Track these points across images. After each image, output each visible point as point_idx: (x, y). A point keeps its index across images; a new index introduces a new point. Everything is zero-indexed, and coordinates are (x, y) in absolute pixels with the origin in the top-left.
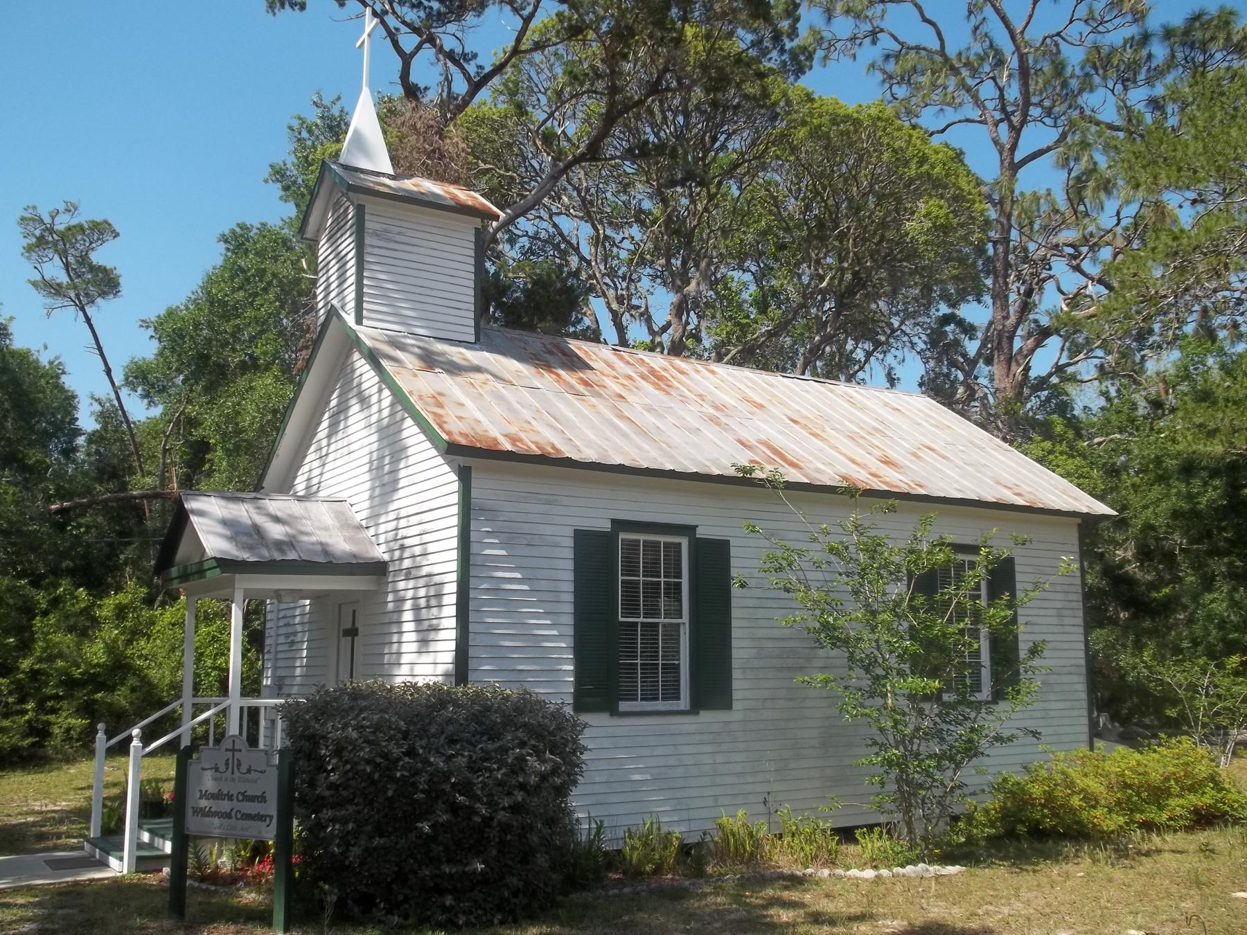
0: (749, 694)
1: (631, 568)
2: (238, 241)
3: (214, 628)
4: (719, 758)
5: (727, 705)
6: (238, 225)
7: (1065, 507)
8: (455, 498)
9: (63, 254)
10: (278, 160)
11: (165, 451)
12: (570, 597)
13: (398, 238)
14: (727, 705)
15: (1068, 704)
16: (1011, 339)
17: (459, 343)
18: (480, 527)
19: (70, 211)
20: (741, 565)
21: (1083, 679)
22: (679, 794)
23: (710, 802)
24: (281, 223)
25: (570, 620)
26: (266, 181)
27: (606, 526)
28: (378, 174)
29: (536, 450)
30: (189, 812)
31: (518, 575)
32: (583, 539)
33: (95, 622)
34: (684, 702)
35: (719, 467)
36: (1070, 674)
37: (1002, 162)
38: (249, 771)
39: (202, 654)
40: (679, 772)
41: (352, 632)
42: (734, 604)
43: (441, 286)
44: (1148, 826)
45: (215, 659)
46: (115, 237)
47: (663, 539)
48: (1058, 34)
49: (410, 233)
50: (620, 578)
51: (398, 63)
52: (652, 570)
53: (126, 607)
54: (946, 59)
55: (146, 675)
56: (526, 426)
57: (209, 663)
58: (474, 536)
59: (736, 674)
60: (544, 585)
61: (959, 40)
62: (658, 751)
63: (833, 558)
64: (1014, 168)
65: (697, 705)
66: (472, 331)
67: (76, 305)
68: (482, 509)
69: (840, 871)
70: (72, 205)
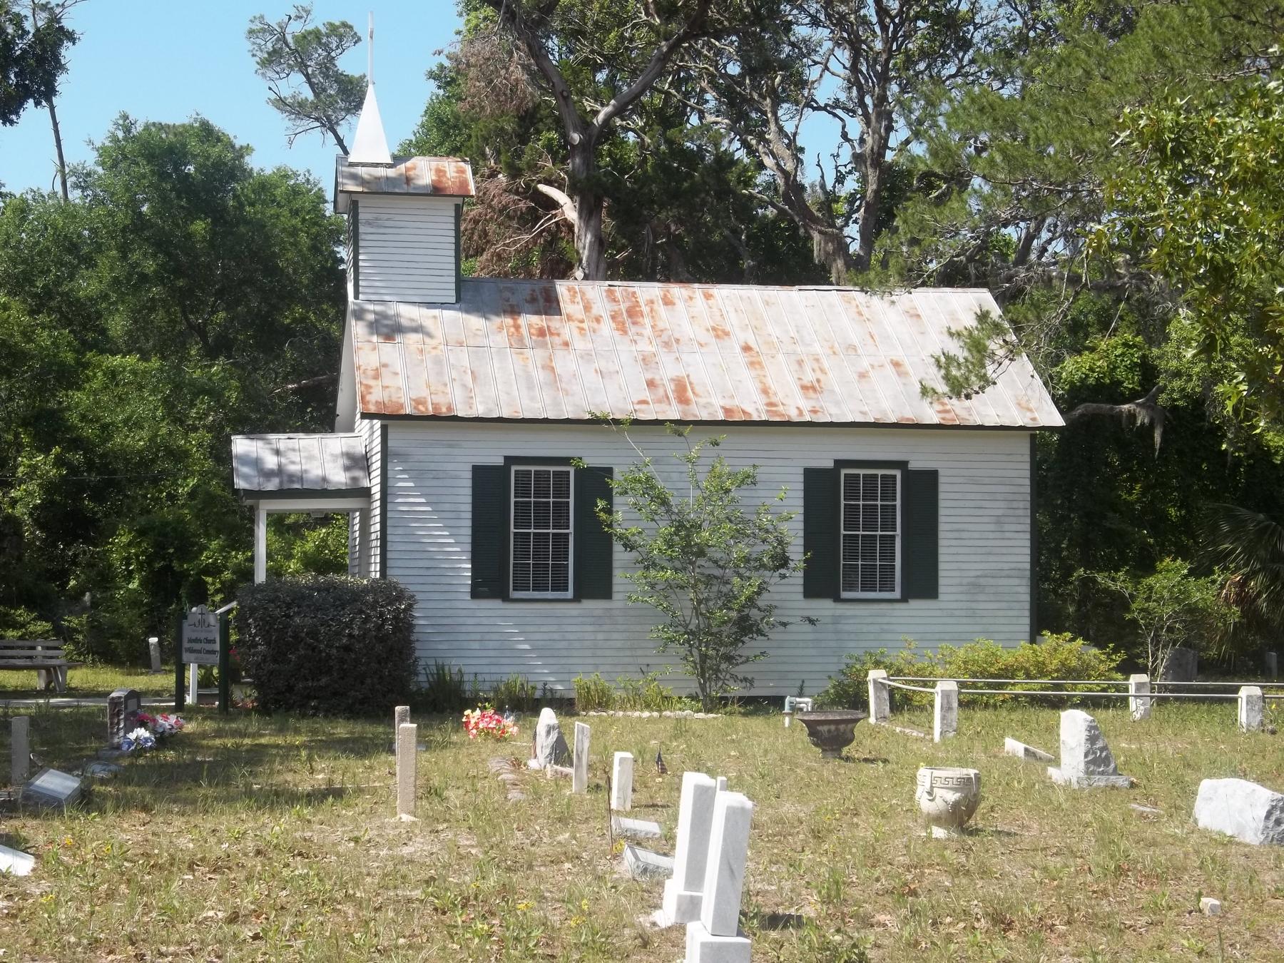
1: (523, 490)
4: (600, 636)
9: (303, 67)
12: (469, 515)
15: (1004, 605)
19: (301, 17)
21: (1026, 582)
22: (563, 661)
29: (431, 412)
31: (423, 500)
34: (570, 594)
36: (1009, 577)
46: (356, 43)
49: (398, 217)
50: (513, 500)
58: (390, 474)
65: (577, 598)
66: (453, 293)
67: (324, 125)
68: (397, 455)
70: (304, 9)
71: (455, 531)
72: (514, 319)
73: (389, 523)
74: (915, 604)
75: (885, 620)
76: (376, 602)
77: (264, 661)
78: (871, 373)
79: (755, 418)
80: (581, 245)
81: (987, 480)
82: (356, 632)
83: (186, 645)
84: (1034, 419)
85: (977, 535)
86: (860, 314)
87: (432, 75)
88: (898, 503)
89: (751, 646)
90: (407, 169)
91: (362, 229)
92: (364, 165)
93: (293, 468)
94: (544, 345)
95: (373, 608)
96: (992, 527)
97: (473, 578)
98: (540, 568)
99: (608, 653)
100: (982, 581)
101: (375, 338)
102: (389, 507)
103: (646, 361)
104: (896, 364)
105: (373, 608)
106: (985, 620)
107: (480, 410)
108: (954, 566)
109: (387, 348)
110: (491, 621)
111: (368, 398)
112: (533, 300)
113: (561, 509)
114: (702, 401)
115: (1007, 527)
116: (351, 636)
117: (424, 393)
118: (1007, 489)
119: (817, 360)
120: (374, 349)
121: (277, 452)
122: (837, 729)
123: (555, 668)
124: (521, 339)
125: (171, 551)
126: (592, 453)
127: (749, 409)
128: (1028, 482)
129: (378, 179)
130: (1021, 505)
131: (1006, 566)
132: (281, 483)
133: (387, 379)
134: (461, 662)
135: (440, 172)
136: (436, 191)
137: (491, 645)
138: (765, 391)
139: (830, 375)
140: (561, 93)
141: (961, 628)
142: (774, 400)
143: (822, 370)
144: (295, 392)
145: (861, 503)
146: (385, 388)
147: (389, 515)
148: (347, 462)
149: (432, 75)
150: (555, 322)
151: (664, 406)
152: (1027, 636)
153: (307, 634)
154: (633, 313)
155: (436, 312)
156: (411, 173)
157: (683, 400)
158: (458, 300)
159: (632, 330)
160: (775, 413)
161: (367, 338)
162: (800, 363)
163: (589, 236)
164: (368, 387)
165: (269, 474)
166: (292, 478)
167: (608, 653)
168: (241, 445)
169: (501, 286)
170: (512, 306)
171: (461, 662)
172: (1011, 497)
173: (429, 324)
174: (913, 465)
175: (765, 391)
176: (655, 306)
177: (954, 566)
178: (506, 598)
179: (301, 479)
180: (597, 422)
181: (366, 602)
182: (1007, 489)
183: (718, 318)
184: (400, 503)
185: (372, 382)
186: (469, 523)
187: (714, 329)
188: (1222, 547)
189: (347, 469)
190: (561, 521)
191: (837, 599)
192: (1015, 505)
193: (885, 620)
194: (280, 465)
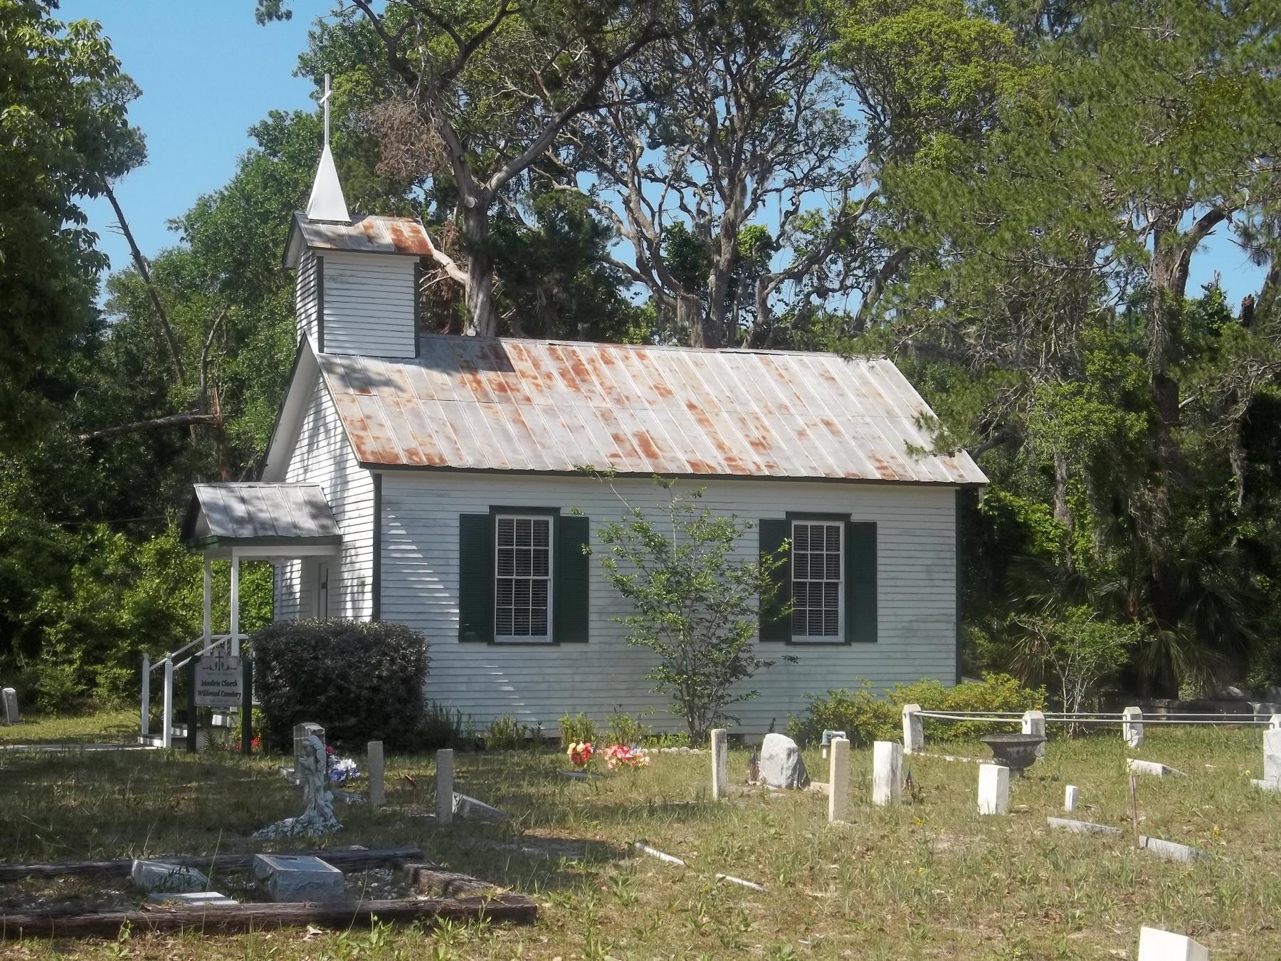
0: (604, 632)
1: (506, 539)
4: (577, 678)
6: (271, 114)
8: (372, 495)
11: (206, 364)
12: (457, 562)
13: (352, 280)
15: (934, 648)
18: (388, 516)
21: (953, 626)
28: (336, 223)
29: (425, 461)
31: (414, 547)
32: (468, 523)
33: (137, 570)
39: (246, 604)
40: (543, 686)
41: (325, 586)
45: (260, 609)
46: (136, 97)
50: (497, 547)
52: (523, 540)
53: (168, 552)
55: (189, 626)
56: (428, 440)
57: (253, 613)
58: (383, 522)
59: (592, 617)
62: (526, 671)
65: (557, 640)
66: (413, 348)
68: (390, 503)
71: (444, 577)
72: (474, 375)
73: (383, 568)
74: (856, 647)
75: (831, 662)
76: (399, 645)
77: (288, 703)
78: (808, 431)
79: (720, 472)
80: (472, 304)
81: (918, 532)
82: (385, 674)
83: (198, 687)
84: (961, 476)
85: (910, 583)
86: (780, 375)
87: (254, 132)
88: (842, 552)
89: (738, 687)
90: (366, 228)
91: (326, 284)
92: (324, 222)
93: (263, 516)
94: (508, 400)
95: (397, 651)
96: (922, 575)
97: (462, 621)
98: (522, 613)
99: (584, 694)
100: (915, 625)
101: (351, 391)
102: (383, 553)
103: (606, 416)
104: (828, 424)
105: (397, 651)
106: (917, 662)
107: (469, 461)
108: (891, 612)
109: (364, 399)
110: (478, 664)
111: (363, 447)
112: (484, 357)
113: (542, 556)
114: (668, 455)
115: (936, 576)
116: (379, 677)
117: (414, 444)
118: (937, 540)
119: (757, 419)
120: (353, 401)
121: (243, 500)
122: (1025, 751)
123: (536, 709)
124: (486, 394)
125: (6, 601)
126: (571, 504)
127: (713, 464)
128: (954, 534)
129: (341, 236)
130: (948, 555)
131: (936, 612)
132: (255, 530)
133: (374, 431)
134: (458, 703)
135: (396, 231)
136: (399, 249)
137: (476, 687)
138: (720, 447)
139: (773, 431)
140: (459, 158)
141: (897, 670)
142: (730, 455)
143: (765, 428)
144: (87, 443)
145: (825, 552)
146: (376, 438)
147: (383, 561)
148: (313, 511)
149: (254, 132)
150: (510, 378)
151: (635, 460)
152: (953, 676)
153: (338, 676)
154: (579, 369)
155: (400, 366)
156: (371, 232)
157: (651, 455)
158: (418, 355)
159: (583, 387)
160: (736, 467)
161: (343, 390)
162: (743, 420)
163: (481, 296)
164: (359, 437)
165: (241, 521)
166: (263, 525)
167: (584, 694)
168: (205, 493)
169: (452, 342)
170: (467, 362)
171: (458, 703)
172: (939, 548)
173: (395, 377)
174: (856, 518)
175: (720, 447)
176: (597, 365)
177: (891, 612)
178: (490, 641)
179: (273, 527)
180: (583, 475)
181: (388, 645)
182: (937, 540)
183: (657, 378)
184: (394, 550)
185: (362, 433)
186: (457, 570)
187: (657, 388)
188: (1029, 598)
189: (314, 517)
190: (541, 568)
191: (789, 642)
192: (942, 555)
193: (831, 662)
194: (249, 514)
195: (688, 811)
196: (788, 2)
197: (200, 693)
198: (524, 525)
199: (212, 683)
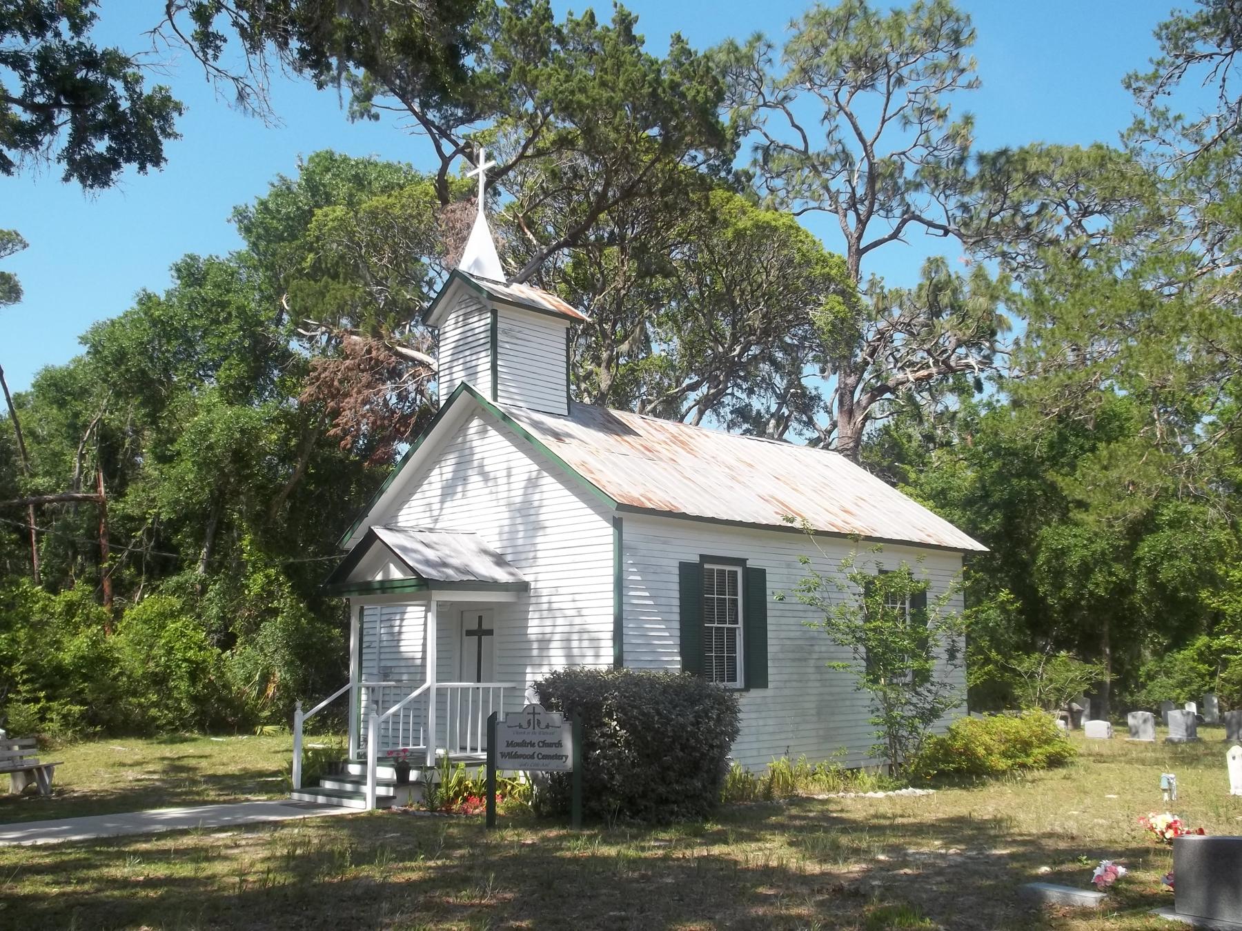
2: (191, 273)
3: (179, 624)
4: (761, 722)
5: (765, 685)
7: (959, 546)
10: (241, 204)
13: (519, 335)
14: (765, 685)
16: (852, 393)
17: (560, 416)
20: (774, 587)
23: (755, 753)
24: (229, 256)
25: (677, 625)
26: (229, 221)
27: (696, 559)
30: (499, 756)
32: (685, 568)
34: (740, 683)
35: (765, 518)
37: (849, 248)
38: (547, 727)
42: (769, 613)
43: (545, 372)
44: (1023, 766)
47: (727, 568)
48: (904, 153)
51: (439, 163)
54: (808, 158)
59: (770, 663)
60: (663, 601)
61: (818, 145)
63: (853, 584)
64: (860, 252)
69: (861, 794)
91: (500, 337)
92: (488, 280)
102: (625, 599)
149: (84, 340)
195: (206, 757)
196: (1, 438)
197: (503, 755)
198: (722, 572)
199: (524, 744)
